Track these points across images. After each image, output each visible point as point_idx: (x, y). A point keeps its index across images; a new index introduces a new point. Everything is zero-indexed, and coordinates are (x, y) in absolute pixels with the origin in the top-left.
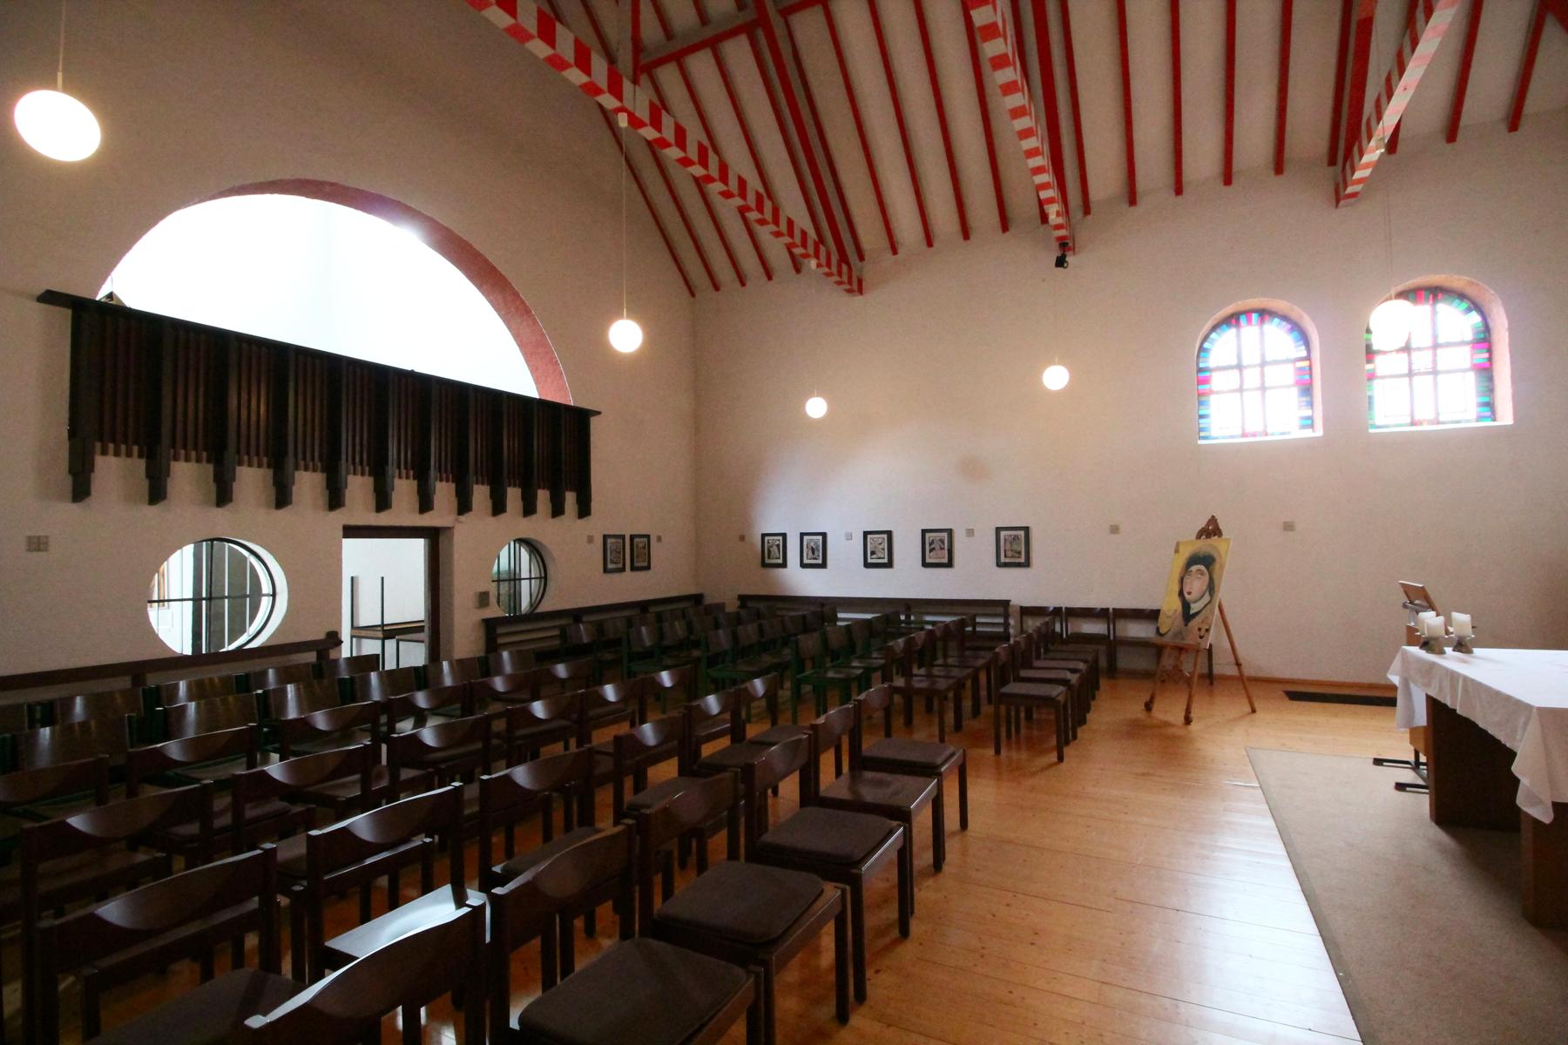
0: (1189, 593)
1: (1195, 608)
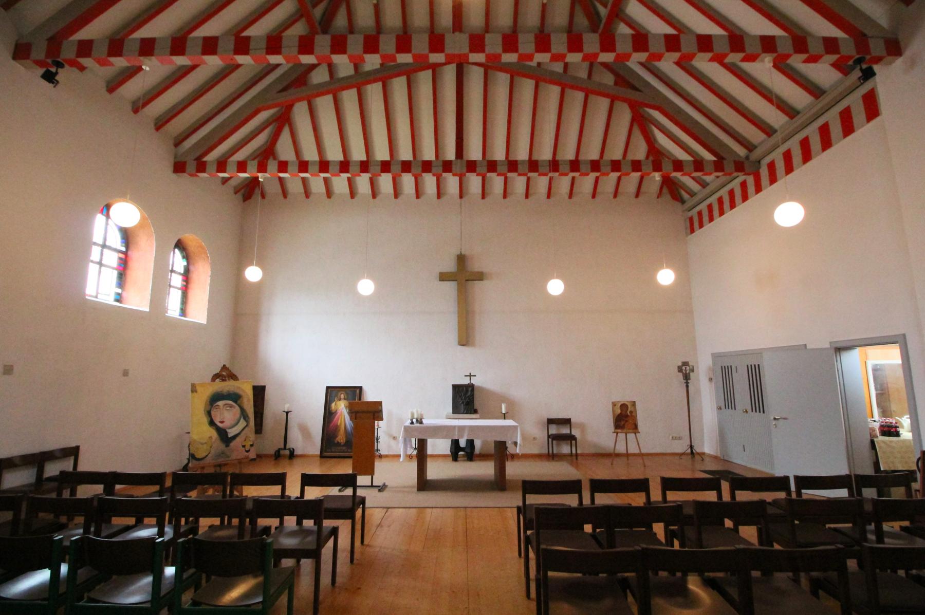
0: (222, 422)
1: (232, 433)
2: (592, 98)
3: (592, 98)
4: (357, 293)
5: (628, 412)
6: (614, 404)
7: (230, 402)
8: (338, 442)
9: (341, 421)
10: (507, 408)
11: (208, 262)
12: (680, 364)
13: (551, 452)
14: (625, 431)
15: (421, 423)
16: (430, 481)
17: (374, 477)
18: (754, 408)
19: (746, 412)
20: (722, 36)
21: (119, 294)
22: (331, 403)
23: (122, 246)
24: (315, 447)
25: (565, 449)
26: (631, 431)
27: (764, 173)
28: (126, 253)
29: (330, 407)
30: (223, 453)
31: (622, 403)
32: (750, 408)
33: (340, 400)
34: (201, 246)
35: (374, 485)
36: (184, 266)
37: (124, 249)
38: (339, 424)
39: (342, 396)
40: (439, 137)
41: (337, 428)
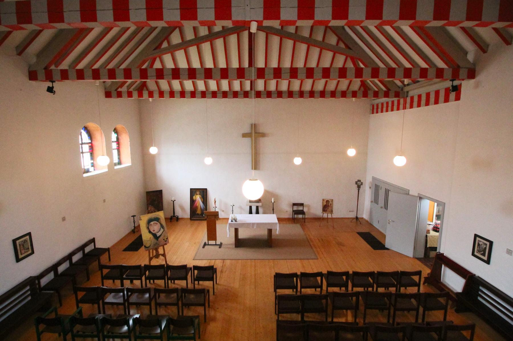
0: (154, 231)
1: (158, 235)
5: (329, 204)
6: (323, 200)
8: (198, 214)
10: (274, 200)
11: (127, 134)
15: (236, 221)
17: (217, 241)
18: (385, 207)
19: (382, 208)
20: (384, 68)
21: (92, 163)
22: (193, 196)
23: (89, 140)
25: (300, 216)
26: (330, 213)
27: (408, 100)
28: (91, 143)
29: (193, 198)
30: (156, 243)
31: (327, 200)
32: (384, 207)
33: (197, 195)
34: (123, 128)
36: (116, 137)
37: (90, 141)
39: (198, 193)
41: (197, 207)
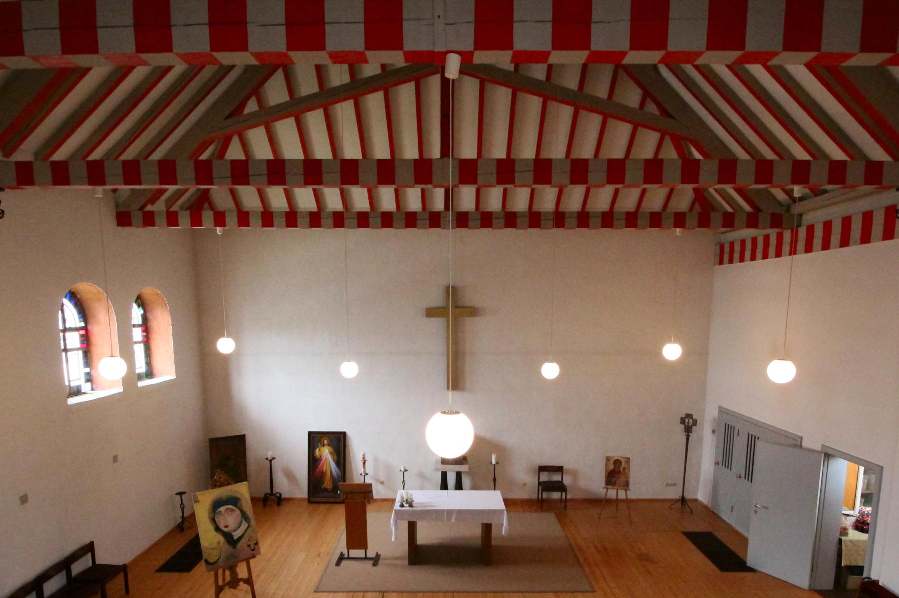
0: (226, 526)
1: (236, 535)
2: (612, 122)
3: (612, 122)
4: (339, 373)
5: (621, 468)
6: (608, 459)
7: (230, 506)
9: (326, 466)
10: (497, 458)
11: (167, 309)
12: (684, 416)
13: (540, 497)
14: (616, 487)
16: (419, 545)
20: (746, 161)
24: (302, 490)
25: (556, 495)
26: (622, 488)
31: (616, 458)
34: (158, 295)
35: (368, 556)
37: (83, 324)
38: (324, 470)
39: (326, 442)
40: (423, 123)
41: (323, 474)
